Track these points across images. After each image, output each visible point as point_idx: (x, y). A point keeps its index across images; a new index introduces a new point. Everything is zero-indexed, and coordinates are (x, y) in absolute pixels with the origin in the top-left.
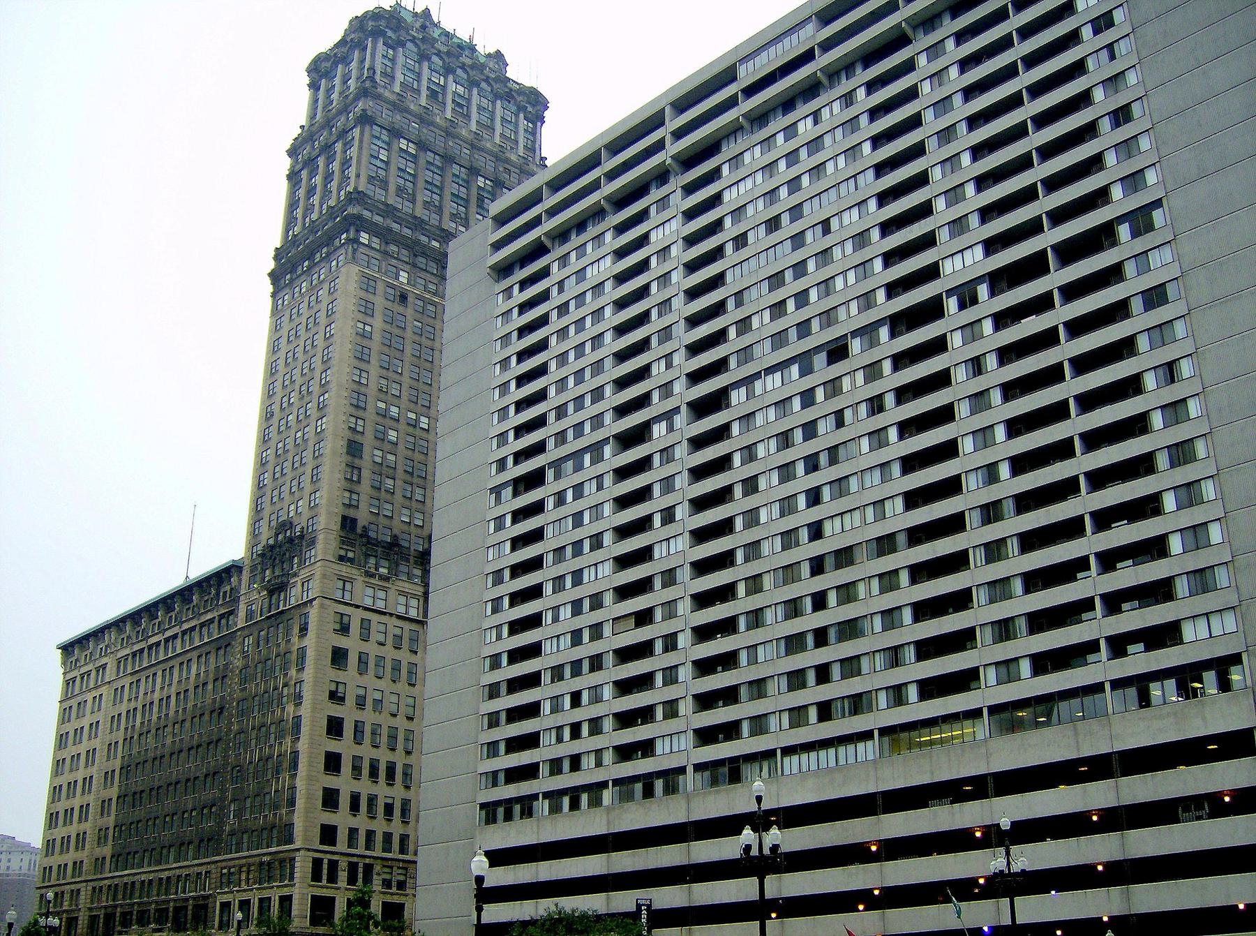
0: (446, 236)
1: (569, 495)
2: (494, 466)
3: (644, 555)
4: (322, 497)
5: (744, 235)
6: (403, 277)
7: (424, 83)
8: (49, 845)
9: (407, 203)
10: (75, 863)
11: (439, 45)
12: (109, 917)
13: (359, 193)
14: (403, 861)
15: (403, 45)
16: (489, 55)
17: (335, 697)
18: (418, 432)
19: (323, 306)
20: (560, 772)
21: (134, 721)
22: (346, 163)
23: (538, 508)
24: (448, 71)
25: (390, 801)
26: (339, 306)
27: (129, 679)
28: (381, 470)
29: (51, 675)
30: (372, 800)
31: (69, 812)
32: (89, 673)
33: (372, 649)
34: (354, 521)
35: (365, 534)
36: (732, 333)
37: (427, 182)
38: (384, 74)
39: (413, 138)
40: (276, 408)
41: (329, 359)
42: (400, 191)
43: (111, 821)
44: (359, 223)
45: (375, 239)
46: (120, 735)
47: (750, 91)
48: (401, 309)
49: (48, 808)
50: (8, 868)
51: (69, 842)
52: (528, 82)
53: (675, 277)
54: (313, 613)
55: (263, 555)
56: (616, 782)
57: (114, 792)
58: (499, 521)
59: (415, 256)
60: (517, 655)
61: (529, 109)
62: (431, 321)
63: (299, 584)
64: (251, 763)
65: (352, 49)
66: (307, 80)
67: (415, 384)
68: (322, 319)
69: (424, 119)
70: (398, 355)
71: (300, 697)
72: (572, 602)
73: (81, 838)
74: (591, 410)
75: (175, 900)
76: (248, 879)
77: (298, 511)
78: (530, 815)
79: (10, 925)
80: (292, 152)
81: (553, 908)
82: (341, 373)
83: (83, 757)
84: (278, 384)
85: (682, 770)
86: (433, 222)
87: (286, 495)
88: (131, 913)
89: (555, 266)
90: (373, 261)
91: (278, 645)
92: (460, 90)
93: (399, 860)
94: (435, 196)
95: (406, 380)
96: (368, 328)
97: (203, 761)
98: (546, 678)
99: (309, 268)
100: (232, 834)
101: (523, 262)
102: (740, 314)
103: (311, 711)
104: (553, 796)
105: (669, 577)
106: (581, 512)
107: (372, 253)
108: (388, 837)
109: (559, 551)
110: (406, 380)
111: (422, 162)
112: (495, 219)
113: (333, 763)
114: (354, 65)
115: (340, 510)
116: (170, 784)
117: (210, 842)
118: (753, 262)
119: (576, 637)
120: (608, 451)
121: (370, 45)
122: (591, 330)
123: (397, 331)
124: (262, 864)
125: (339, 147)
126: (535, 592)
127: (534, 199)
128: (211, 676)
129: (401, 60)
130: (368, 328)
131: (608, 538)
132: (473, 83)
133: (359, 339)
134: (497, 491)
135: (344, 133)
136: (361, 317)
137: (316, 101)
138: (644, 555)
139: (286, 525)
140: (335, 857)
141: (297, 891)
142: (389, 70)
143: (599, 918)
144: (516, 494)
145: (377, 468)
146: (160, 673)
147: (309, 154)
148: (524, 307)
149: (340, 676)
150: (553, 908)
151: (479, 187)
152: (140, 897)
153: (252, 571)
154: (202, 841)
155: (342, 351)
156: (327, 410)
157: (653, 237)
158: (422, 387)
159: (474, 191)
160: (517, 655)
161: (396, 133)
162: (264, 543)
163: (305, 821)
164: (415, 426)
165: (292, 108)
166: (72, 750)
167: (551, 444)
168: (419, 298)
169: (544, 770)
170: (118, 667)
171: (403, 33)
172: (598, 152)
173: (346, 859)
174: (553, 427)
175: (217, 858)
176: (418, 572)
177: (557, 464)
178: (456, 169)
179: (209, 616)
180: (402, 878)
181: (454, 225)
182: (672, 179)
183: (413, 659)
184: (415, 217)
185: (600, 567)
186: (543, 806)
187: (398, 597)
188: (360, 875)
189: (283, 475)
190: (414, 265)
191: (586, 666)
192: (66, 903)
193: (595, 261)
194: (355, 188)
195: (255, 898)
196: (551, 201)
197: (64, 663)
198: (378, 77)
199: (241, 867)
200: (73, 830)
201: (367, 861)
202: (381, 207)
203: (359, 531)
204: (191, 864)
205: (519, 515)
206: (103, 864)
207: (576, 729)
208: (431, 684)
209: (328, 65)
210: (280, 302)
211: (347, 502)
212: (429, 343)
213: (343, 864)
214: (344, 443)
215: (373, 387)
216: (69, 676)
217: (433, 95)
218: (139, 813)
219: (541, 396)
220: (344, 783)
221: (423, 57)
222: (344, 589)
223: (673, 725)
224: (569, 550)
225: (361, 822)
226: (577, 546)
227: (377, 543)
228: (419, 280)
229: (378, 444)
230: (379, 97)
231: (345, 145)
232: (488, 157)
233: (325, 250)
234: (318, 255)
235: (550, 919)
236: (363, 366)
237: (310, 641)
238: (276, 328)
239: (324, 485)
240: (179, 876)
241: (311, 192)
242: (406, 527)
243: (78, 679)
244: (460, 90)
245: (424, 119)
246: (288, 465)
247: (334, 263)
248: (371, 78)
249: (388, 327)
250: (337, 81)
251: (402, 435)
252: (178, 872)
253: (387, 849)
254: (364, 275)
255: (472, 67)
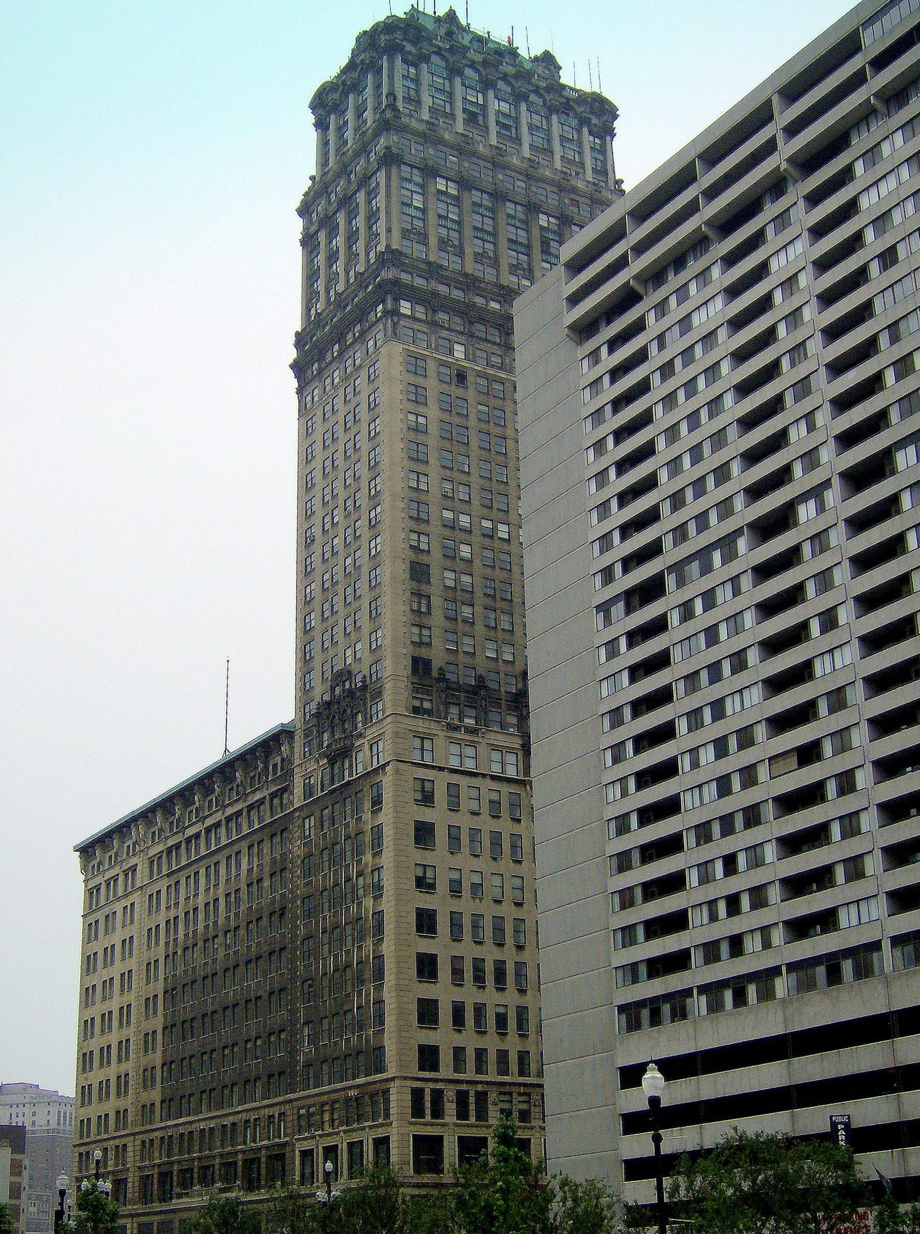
0: (508, 295)
1: (698, 605)
2: (599, 577)
3: (801, 673)
4: (385, 636)
5: (892, 250)
6: (459, 351)
7: (459, 105)
8: (85, 1092)
9: (454, 258)
10: (118, 1112)
11: (471, 54)
12: (165, 1176)
13: (393, 252)
14: (525, 1085)
15: (427, 60)
16: (536, 59)
17: (423, 884)
18: (497, 544)
19: (363, 397)
20: (717, 959)
21: (176, 932)
22: (372, 217)
23: (658, 626)
24: (487, 85)
25: (501, 1010)
26: (383, 396)
27: (165, 883)
28: (455, 595)
29: (70, 883)
30: (479, 1010)
31: (106, 1051)
32: (115, 879)
33: (464, 821)
34: (427, 663)
35: (442, 678)
36: (890, 377)
37: (475, 228)
38: (408, 99)
39: (452, 174)
40: (317, 531)
41: (377, 464)
42: (443, 243)
43: (157, 1058)
44: (398, 290)
45: (419, 308)
46: (160, 952)
47: (880, 62)
48: (460, 392)
49: (80, 1048)
50: (34, 1123)
51: (108, 1087)
52: (584, 86)
53: (807, 314)
54: (387, 781)
55: (318, 715)
56: (793, 967)
57: (158, 1023)
58: (612, 647)
59: (471, 323)
60: (651, 814)
61: (595, 121)
62: (499, 403)
63: (367, 746)
64: (325, 974)
65: (364, 72)
66: (312, 119)
67: (487, 484)
68: (364, 414)
69: (463, 150)
70: (462, 449)
71: (380, 888)
72: (715, 741)
73: (123, 1082)
74: (715, 494)
75: (243, 1152)
76: (332, 1120)
77: (356, 656)
78: (684, 1016)
79: (62, 1193)
80: (304, 210)
81: (732, 1133)
82: (393, 481)
83: (117, 982)
84: (317, 502)
85: (875, 946)
86: (452, 266)
87: (340, 638)
88: (191, 1170)
89: (651, 318)
90: (419, 335)
91: (347, 825)
92: (505, 107)
93: (520, 1085)
94: (487, 245)
95: (474, 479)
96: (421, 420)
97: (265, 977)
98: (689, 840)
99: (341, 353)
100: (308, 1065)
101: (609, 317)
102: (898, 352)
103: (395, 905)
104: (712, 990)
105: (837, 699)
106: (716, 626)
107: (416, 326)
108: (503, 1055)
109: (691, 679)
110: (474, 479)
111: (467, 204)
112: (568, 265)
113: (427, 967)
114: (369, 92)
115: (408, 651)
116: (225, 1008)
117: (279, 1077)
118: (908, 282)
119: (724, 786)
120: (742, 544)
121: (385, 65)
122: (705, 392)
123: (457, 420)
124: (348, 1099)
125: (361, 197)
126: (666, 733)
127: (615, 234)
128: (267, 869)
129: (426, 78)
130: (421, 420)
131: (753, 656)
132: (519, 97)
133: (412, 435)
134: (604, 608)
135: (365, 180)
136: (411, 406)
137: (326, 143)
138: (801, 673)
139: (345, 675)
140: (439, 1086)
141: (394, 1131)
142: (413, 93)
143: (790, 1142)
144: (629, 610)
145: (450, 594)
146: (202, 871)
147: (323, 212)
148: (616, 373)
149: (427, 857)
150: (732, 1133)
151: (542, 228)
152: (201, 1151)
153: (306, 736)
154: (270, 1076)
155: (392, 453)
156: (381, 527)
157: (774, 265)
158: (496, 487)
159: (536, 233)
160: (651, 814)
161: (430, 172)
162: (318, 699)
163: (398, 1041)
164: (492, 537)
165: (295, 156)
166: (104, 974)
167: (668, 542)
168: (479, 375)
169: (696, 958)
170: (151, 871)
171: (425, 44)
172: (691, 165)
173: (452, 1086)
174: (669, 520)
175: (292, 1096)
176: (512, 720)
177: (678, 568)
178: (510, 208)
179: (258, 796)
180: (524, 1106)
181: (514, 279)
182: (791, 189)
183: (517, 829)
184: (466, 275)
185: (746, 693)
186: (699, 1003)
187: (493, 753)
188: (472, 1107)
189: (333, 613)
190: (471, 335)
191: (739, 821)
192: (110, 1163)
193: (703, 304)
194: (388, 247)
195: (342, 1142)
196: (637, 235)
197: (84, 869)
198: (400, 105)
199: (323, 1105)
200: (112, 1071)
201: (480, 1088)
202: (422, 266)
203: (435, 674)
204: (258, 1105)
205: (637, 636)
206: (152, 1112)
207: (733, 902)
208: (546, 859)
209: (336, 96)
210: (309, 398)
211: (417, 639)
212: (498, 431)
213: (450, 1093)
214: (406, 566)
215: (435, 491)
216: (92, 884)
217: (471, 118)
218: (192, 1045)
219: (650, 483)
220: (442, 991)
221: (454, 72)
222: (422, 750)
223: (859, 889)
224: (704, 676)
225: (469, 1040)
226: (714, 670)
227: (459, 687)
228: (478, 353)
229: (448, 563)
230: (404, 129)
231: (368, 193)
232: (549, 188)
233: (358, 328)
234: (350, 335)
235: (728, 1146)
236: (421, 468)
237: (386, 817)
238: (306, 431)
239: (387, 619)
240: (247, 1121)
241: (332, 257)
242: (492, 665)
243: (103, 887)
244: (505, 107)
245: (463, 150)
246: (339, 600)
247: (371, 343)
248: (392, 107)
249: (446, 417)
250: (350, 115)
251: (476, 548)
252: (244, 1116)
253: (503, 1068)
254: (410, 354)
255: (517, 76)
